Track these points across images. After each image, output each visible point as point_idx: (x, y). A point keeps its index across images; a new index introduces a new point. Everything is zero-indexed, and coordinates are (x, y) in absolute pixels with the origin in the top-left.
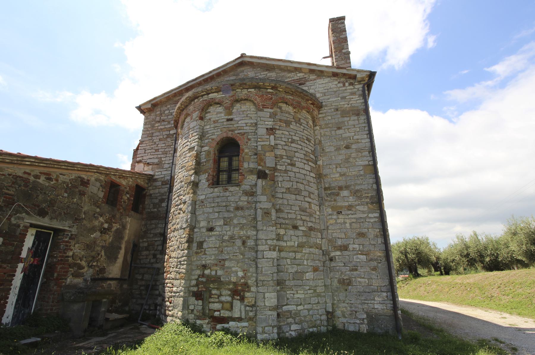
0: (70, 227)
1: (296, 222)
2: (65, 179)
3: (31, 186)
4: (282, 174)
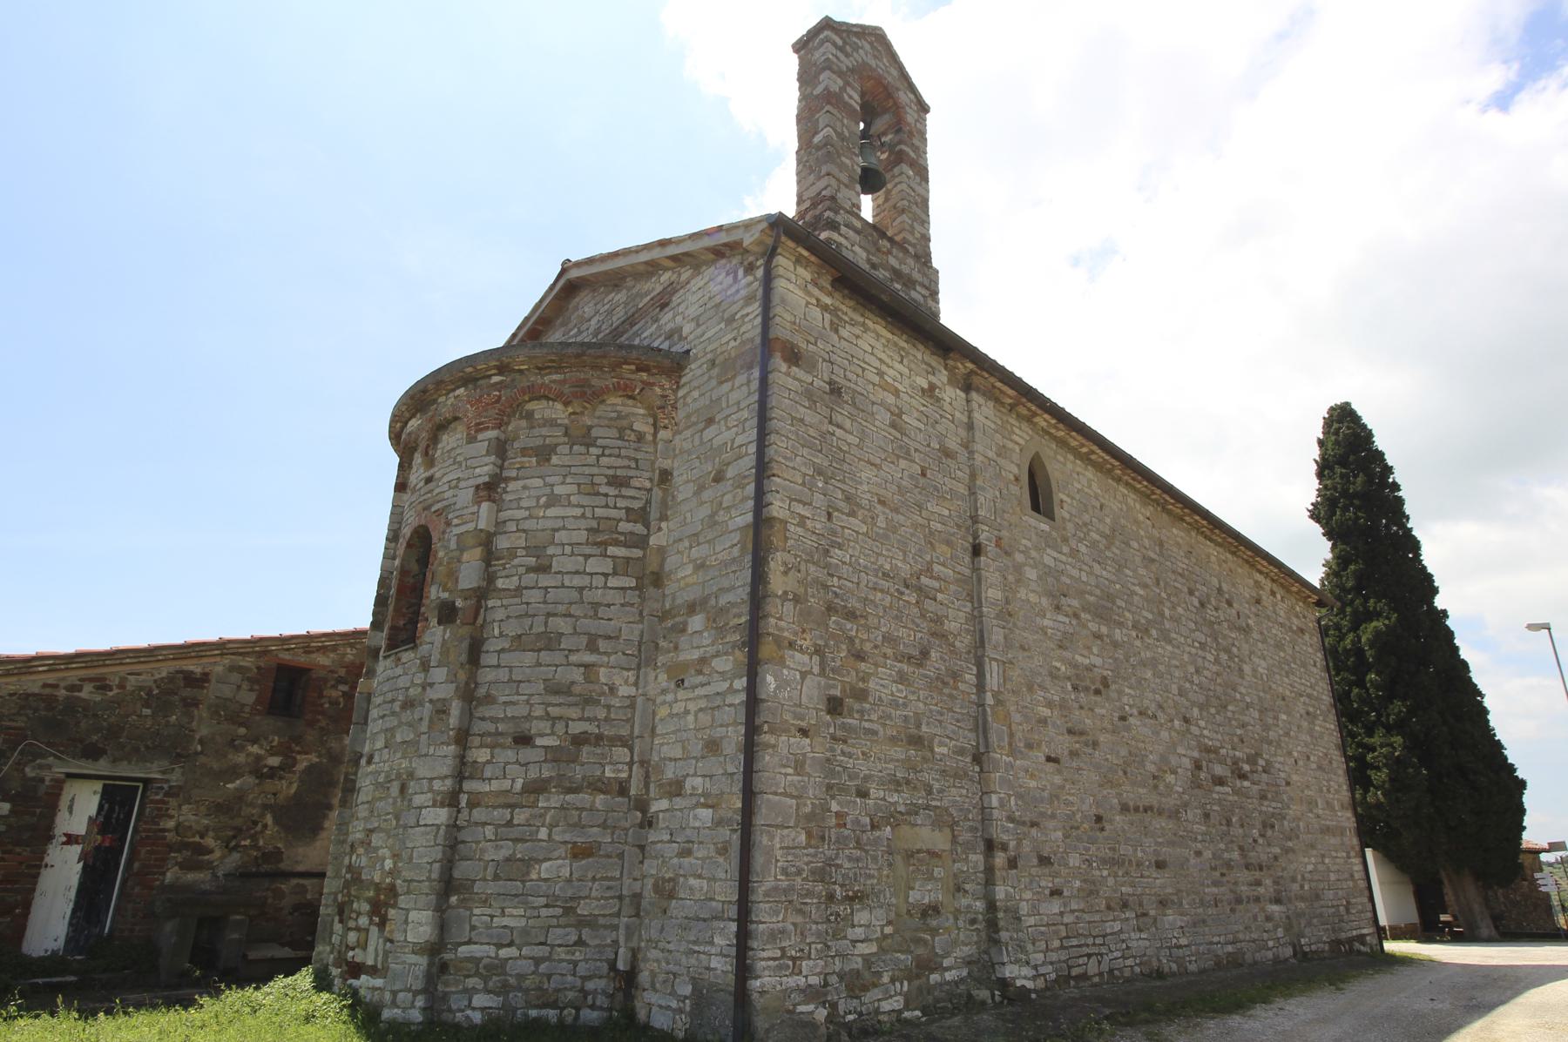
0: (163, 773)
1: (527, 726)
2: (143, 681)
3: (61, 707)
4: (505, 602)
